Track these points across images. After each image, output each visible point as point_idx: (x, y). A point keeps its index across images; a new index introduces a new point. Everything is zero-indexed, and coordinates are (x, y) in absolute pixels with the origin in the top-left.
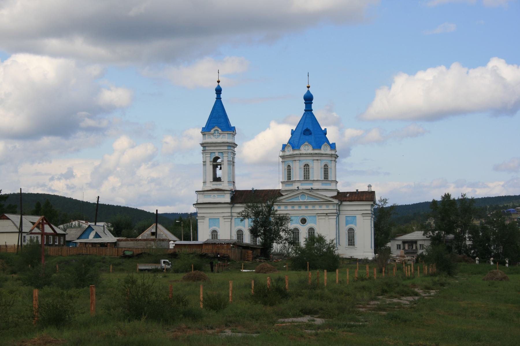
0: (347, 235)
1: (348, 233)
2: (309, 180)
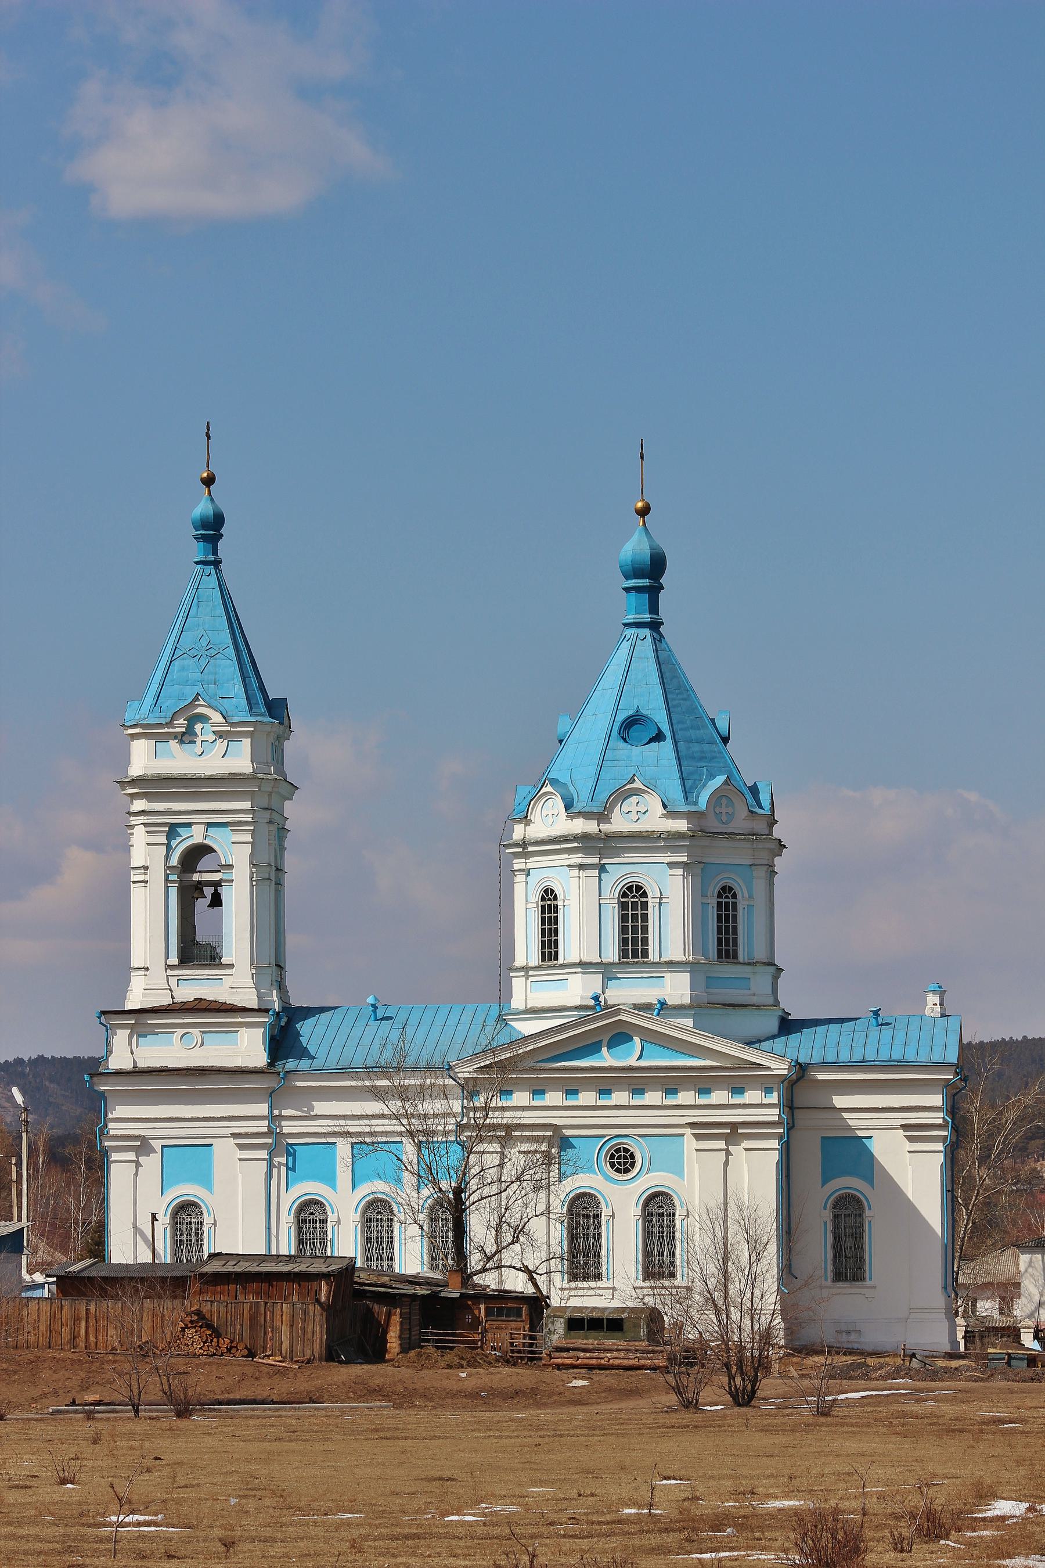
0: (830, 1227)
1: (835, 1216)
2: (555, 967)
